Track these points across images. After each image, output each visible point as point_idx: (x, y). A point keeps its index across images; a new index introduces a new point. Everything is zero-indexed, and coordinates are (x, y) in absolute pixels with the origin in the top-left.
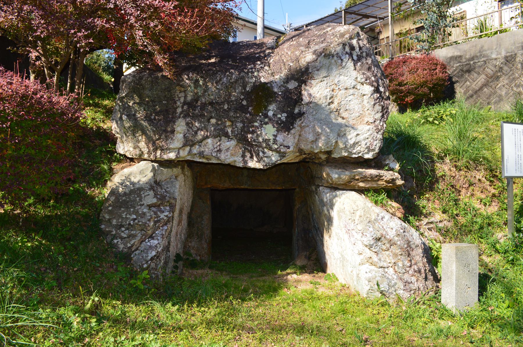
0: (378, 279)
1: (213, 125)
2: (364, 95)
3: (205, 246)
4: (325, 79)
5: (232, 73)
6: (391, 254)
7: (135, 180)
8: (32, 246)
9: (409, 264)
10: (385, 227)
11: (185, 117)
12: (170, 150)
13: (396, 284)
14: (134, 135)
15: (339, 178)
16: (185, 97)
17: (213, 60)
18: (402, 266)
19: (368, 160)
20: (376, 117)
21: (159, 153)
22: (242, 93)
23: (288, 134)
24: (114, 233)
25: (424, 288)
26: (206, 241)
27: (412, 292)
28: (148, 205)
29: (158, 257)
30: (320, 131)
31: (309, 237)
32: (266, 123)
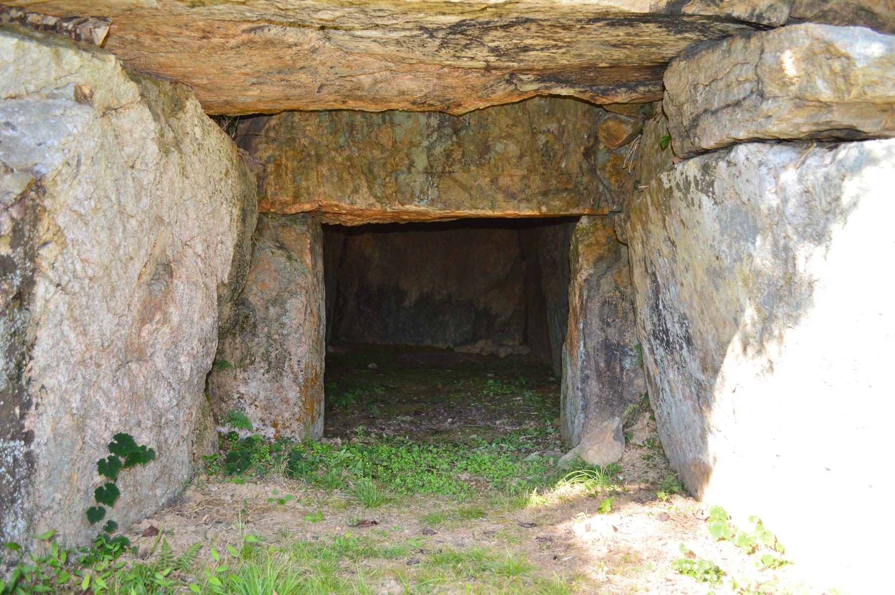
3: (293, 393)
26: (297, 378)
31: (622, 369)
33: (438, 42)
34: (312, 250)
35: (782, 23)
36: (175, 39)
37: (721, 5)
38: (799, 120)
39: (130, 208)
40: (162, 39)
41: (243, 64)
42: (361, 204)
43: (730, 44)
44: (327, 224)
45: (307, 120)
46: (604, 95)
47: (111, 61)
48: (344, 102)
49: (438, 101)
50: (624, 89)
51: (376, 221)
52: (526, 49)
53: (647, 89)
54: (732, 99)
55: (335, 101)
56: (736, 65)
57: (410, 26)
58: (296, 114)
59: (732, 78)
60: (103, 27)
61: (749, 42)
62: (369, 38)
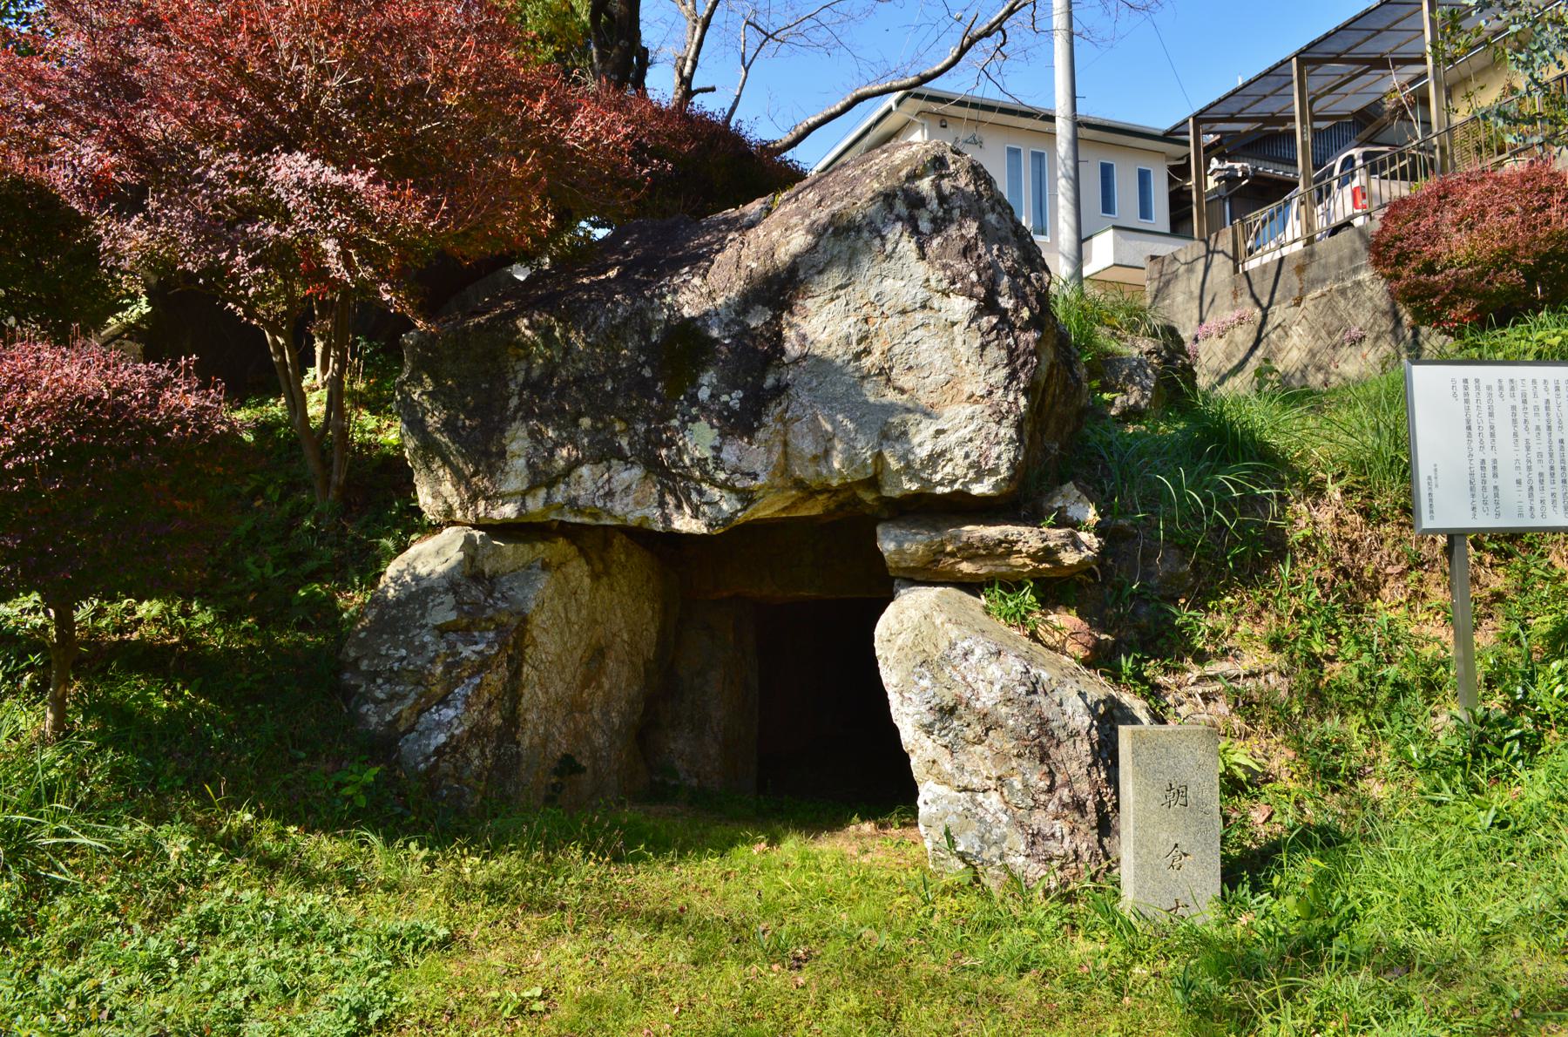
0: (952, 820)
1: (586, 433)
2: (953, 324)
4: (842, 292)
5: (617, 304)
6: (988, 753)
7: (422, 570)
8: (170, 709)
9: (1044, 784)
10: (969, 679)
11: (525, 419)
12: (505, 498)
13: (1004, 837)
14: (429, 468)
15: (900, 551)
16: (528, 371)
17: (612, 274)
18: (1020, 787)
19: (983, 499)
20: (992, 381)
21: (482, 504)
22: (641, 350)
23: (750, 444)
24: (362, 690)
25: (1094, 854)
27: (1056, 864)
28: (436, 627)
29: (455, 749)
30: (829, 427)
32: (695, 419)
39: (573, 618)
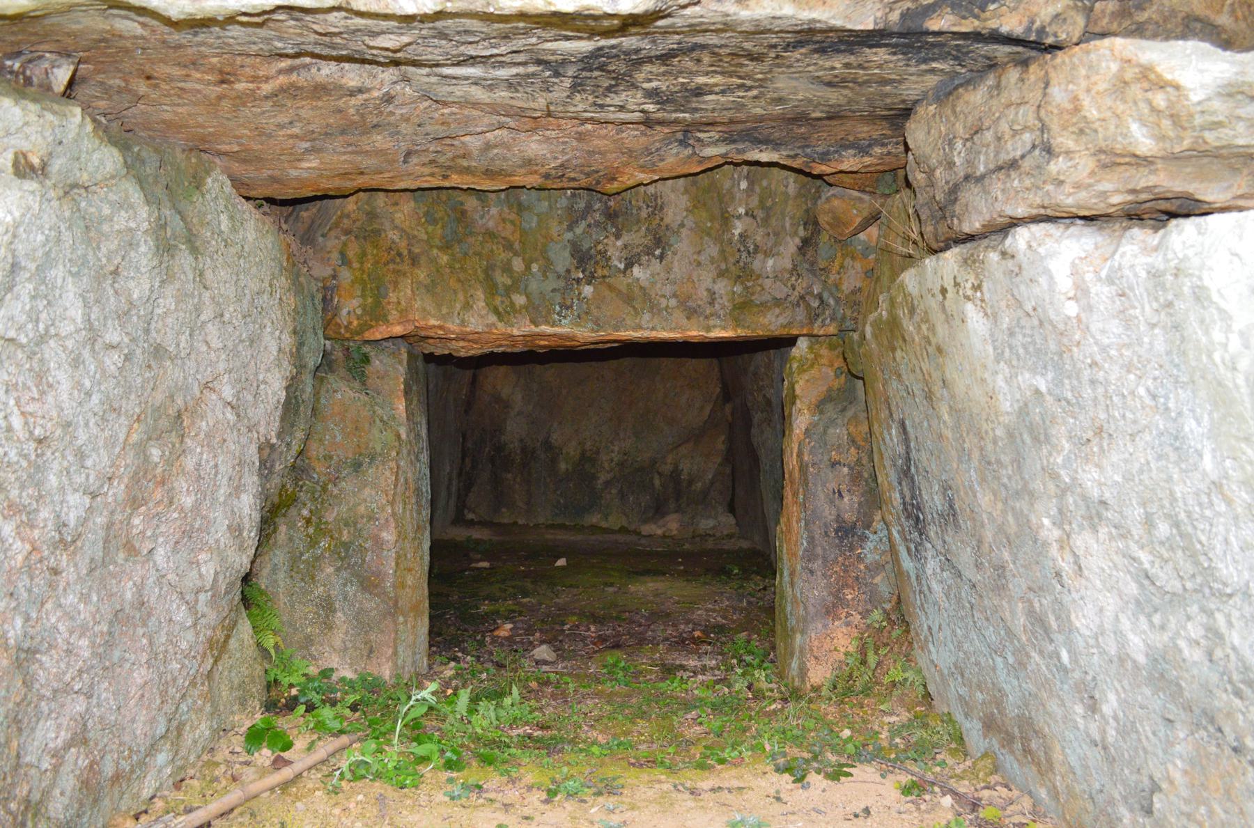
33: (567, 83)
34: (407, 392)
35: (1075, 40)
36: (180, 85)
37: (983, 15)
38: (1106, 186)
40: (164, 86)
41: (286, 120)
42: (473, 323)
43: (1000, 76)
44: (432, 354)
45: (397, 204)
46: (823, 159)
47: (75, 116)
48: (445, 177)
49: (581, 172)
50: (851, 152)
51: (501, 350)
52: (699, 92)
53: (885, 150)
54: (1004, 157)
55: (432, 175)
56: (1008, 106)
57: (521, 58)
58: (381, 194)
59: (1004, 126)
60: (65, 67)
61: (1026, 71)
62: (467, 78)
